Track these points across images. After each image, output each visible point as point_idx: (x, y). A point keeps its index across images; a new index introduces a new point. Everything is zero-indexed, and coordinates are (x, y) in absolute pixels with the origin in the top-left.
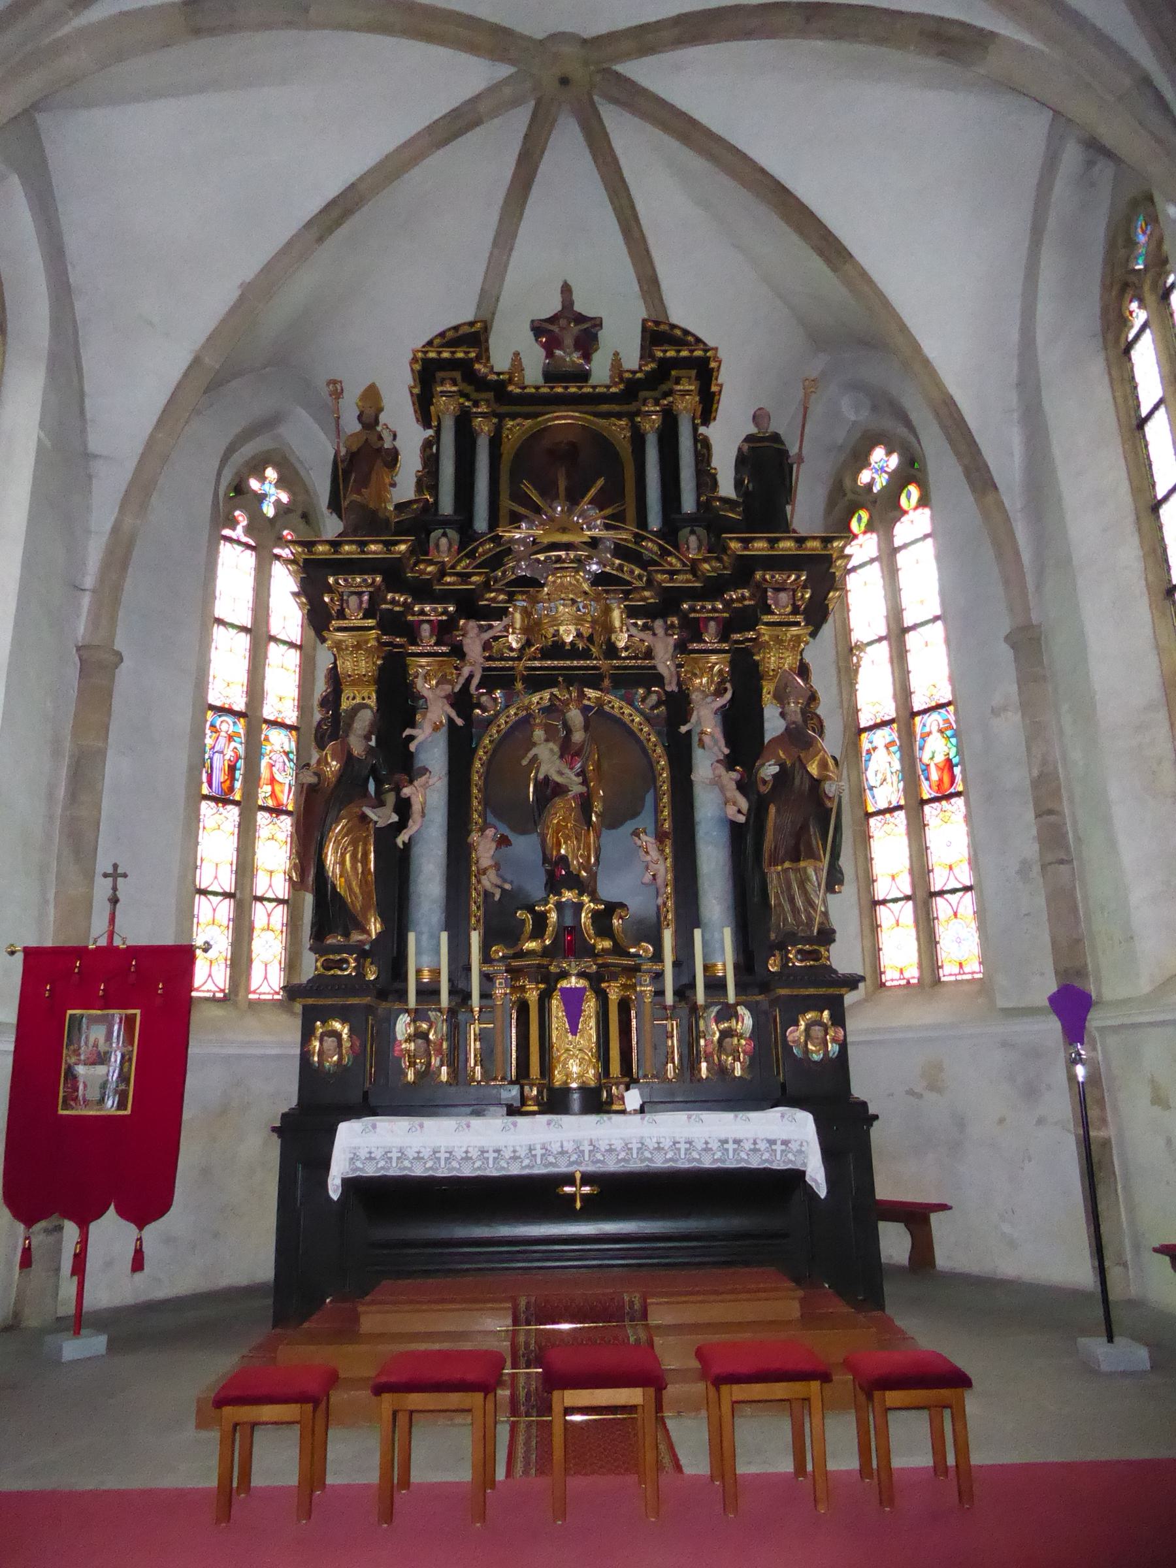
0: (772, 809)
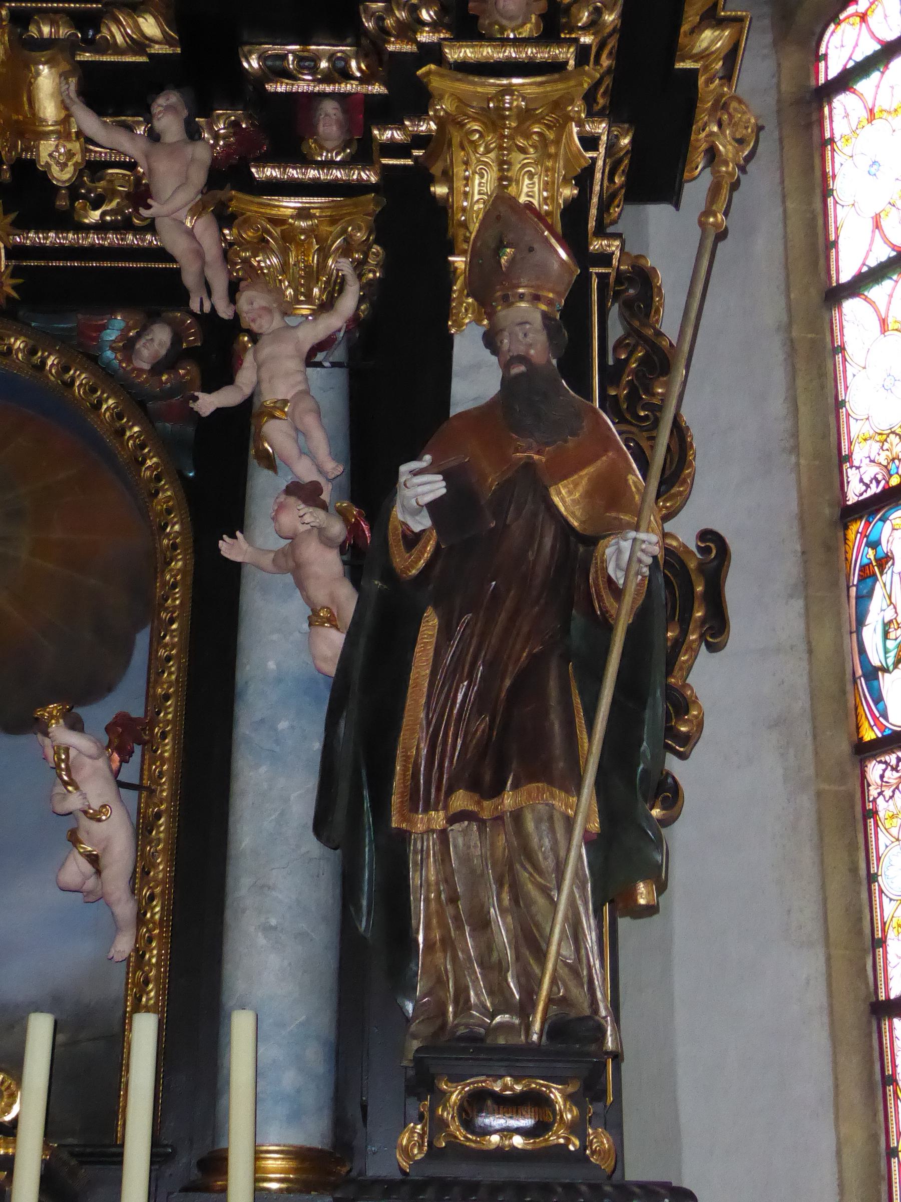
0: (430, 625)
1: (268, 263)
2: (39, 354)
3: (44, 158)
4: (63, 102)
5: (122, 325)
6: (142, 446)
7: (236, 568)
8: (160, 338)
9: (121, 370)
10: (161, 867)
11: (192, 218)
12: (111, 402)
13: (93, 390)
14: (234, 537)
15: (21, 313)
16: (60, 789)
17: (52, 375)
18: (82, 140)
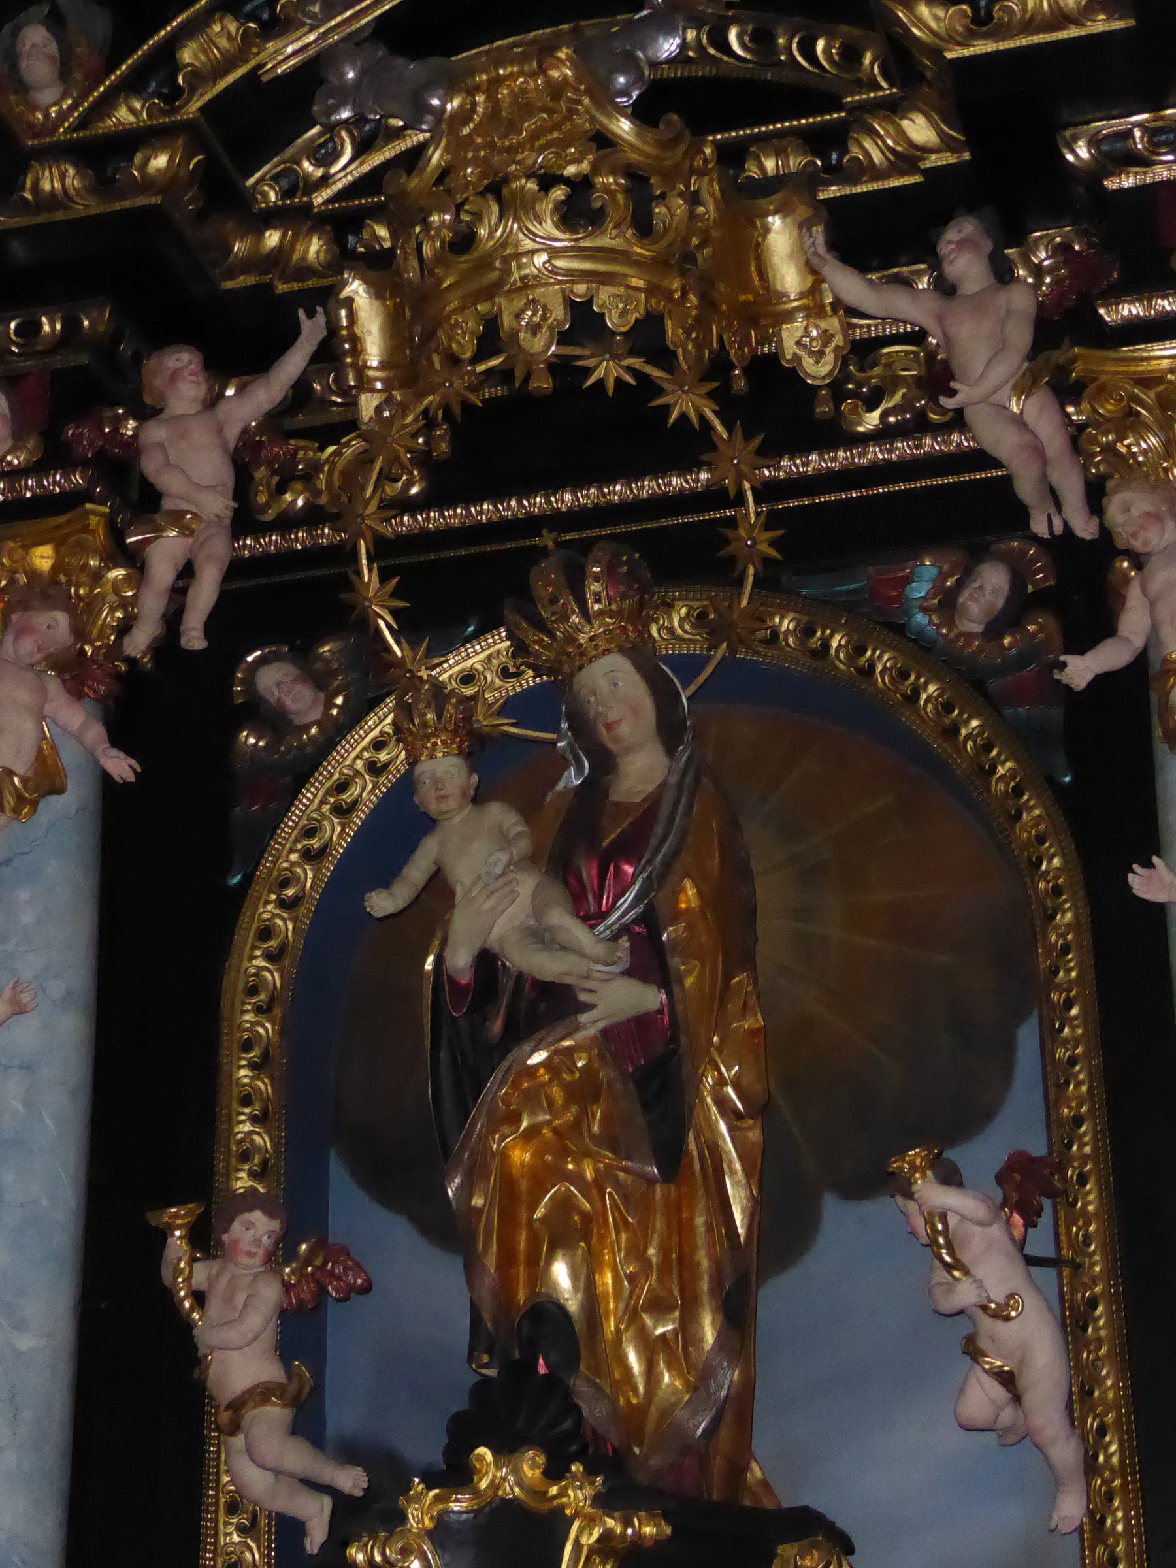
1: (1144, 445)
2: (819, 634)
3: (790, 348)
4: (808, 263)
5: (934, 571)
6: (988, 747)
7: (1158, 911)
8: (992, 584)
9: (941, 639)
10: (1109, 1383)
11: (1019, 399)
12: (932, 688)
13: (904, 675)
14: (1149, 865)
15: (785, 579)
16: (941, 1275)
17: (840, 661)
18: (841, 313)
